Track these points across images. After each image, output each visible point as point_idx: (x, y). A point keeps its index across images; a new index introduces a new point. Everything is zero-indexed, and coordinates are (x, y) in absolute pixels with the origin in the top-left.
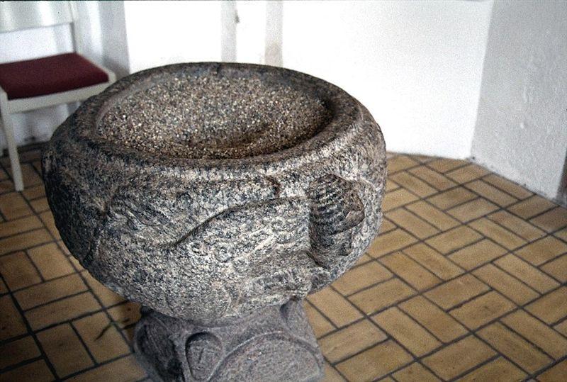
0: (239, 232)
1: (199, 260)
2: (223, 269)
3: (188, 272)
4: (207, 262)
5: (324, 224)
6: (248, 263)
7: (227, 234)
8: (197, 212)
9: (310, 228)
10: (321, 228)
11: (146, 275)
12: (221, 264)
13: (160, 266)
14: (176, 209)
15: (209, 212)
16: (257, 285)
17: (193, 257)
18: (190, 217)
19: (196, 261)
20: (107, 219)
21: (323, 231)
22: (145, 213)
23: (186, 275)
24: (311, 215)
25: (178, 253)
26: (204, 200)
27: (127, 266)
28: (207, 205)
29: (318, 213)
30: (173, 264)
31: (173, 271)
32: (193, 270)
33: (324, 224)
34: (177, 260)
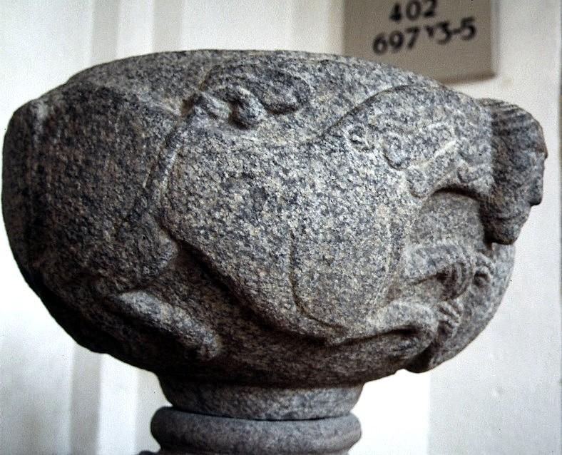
0: (417, 115)
1: (361, 158)
2: (395, 180)
3: (342, 181)
4: (372, 162)
5: (518, 130)
6: (427, 177)
7: (402, 116)
8: (351, 89)
9: (494, 146)
10: (512, 137)
11: (265, 197)
12: (392, 170)
13: (294, 174)
14: (323, 75)
15: (369, 90)
16: (417, 256)
17: (352, 152)
18: (340, 96)
19: (357, 162)
20: (194, 113)
21: (517, 140)
22: (271, 83)
23: (338, 187)
24: (494, 124)
25: (328, 144)
26: (359, 73)
27: (227, 187)
28: (364, 80)
29: (505, 117)
30: (318, 166)
31: (317, 181)
32: (351, 178)
33: (518, 130)
34: (325, 158)
